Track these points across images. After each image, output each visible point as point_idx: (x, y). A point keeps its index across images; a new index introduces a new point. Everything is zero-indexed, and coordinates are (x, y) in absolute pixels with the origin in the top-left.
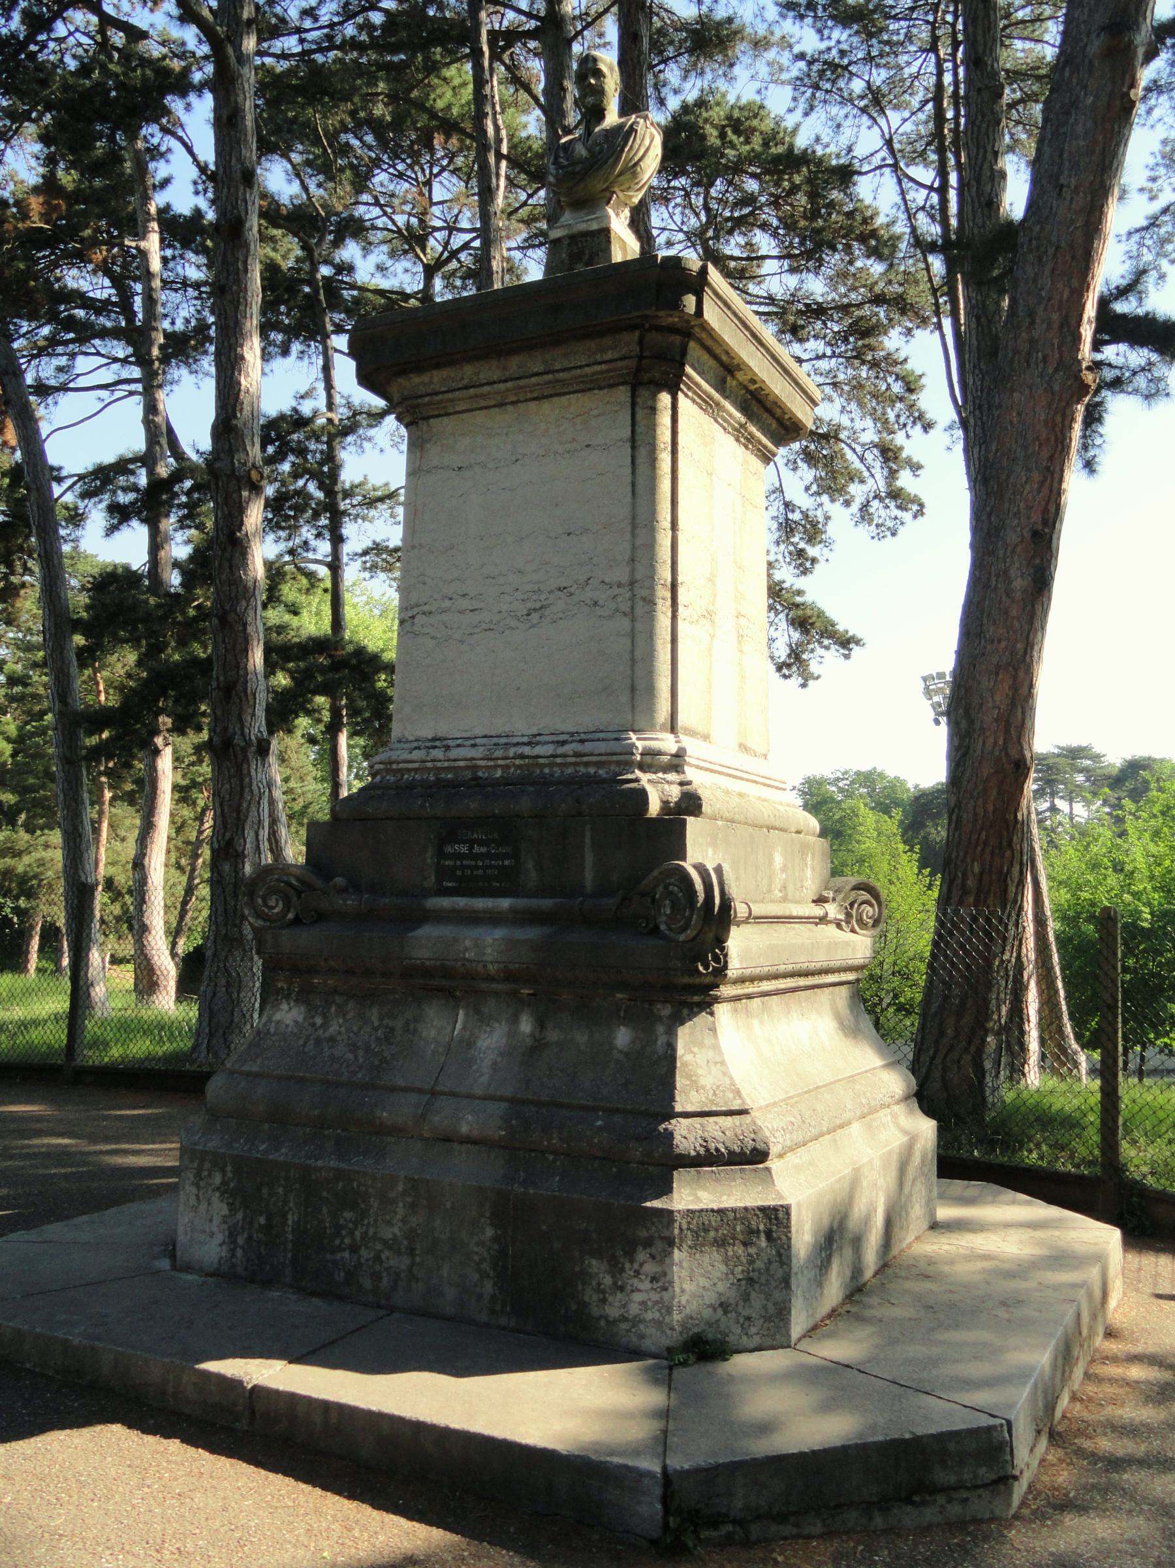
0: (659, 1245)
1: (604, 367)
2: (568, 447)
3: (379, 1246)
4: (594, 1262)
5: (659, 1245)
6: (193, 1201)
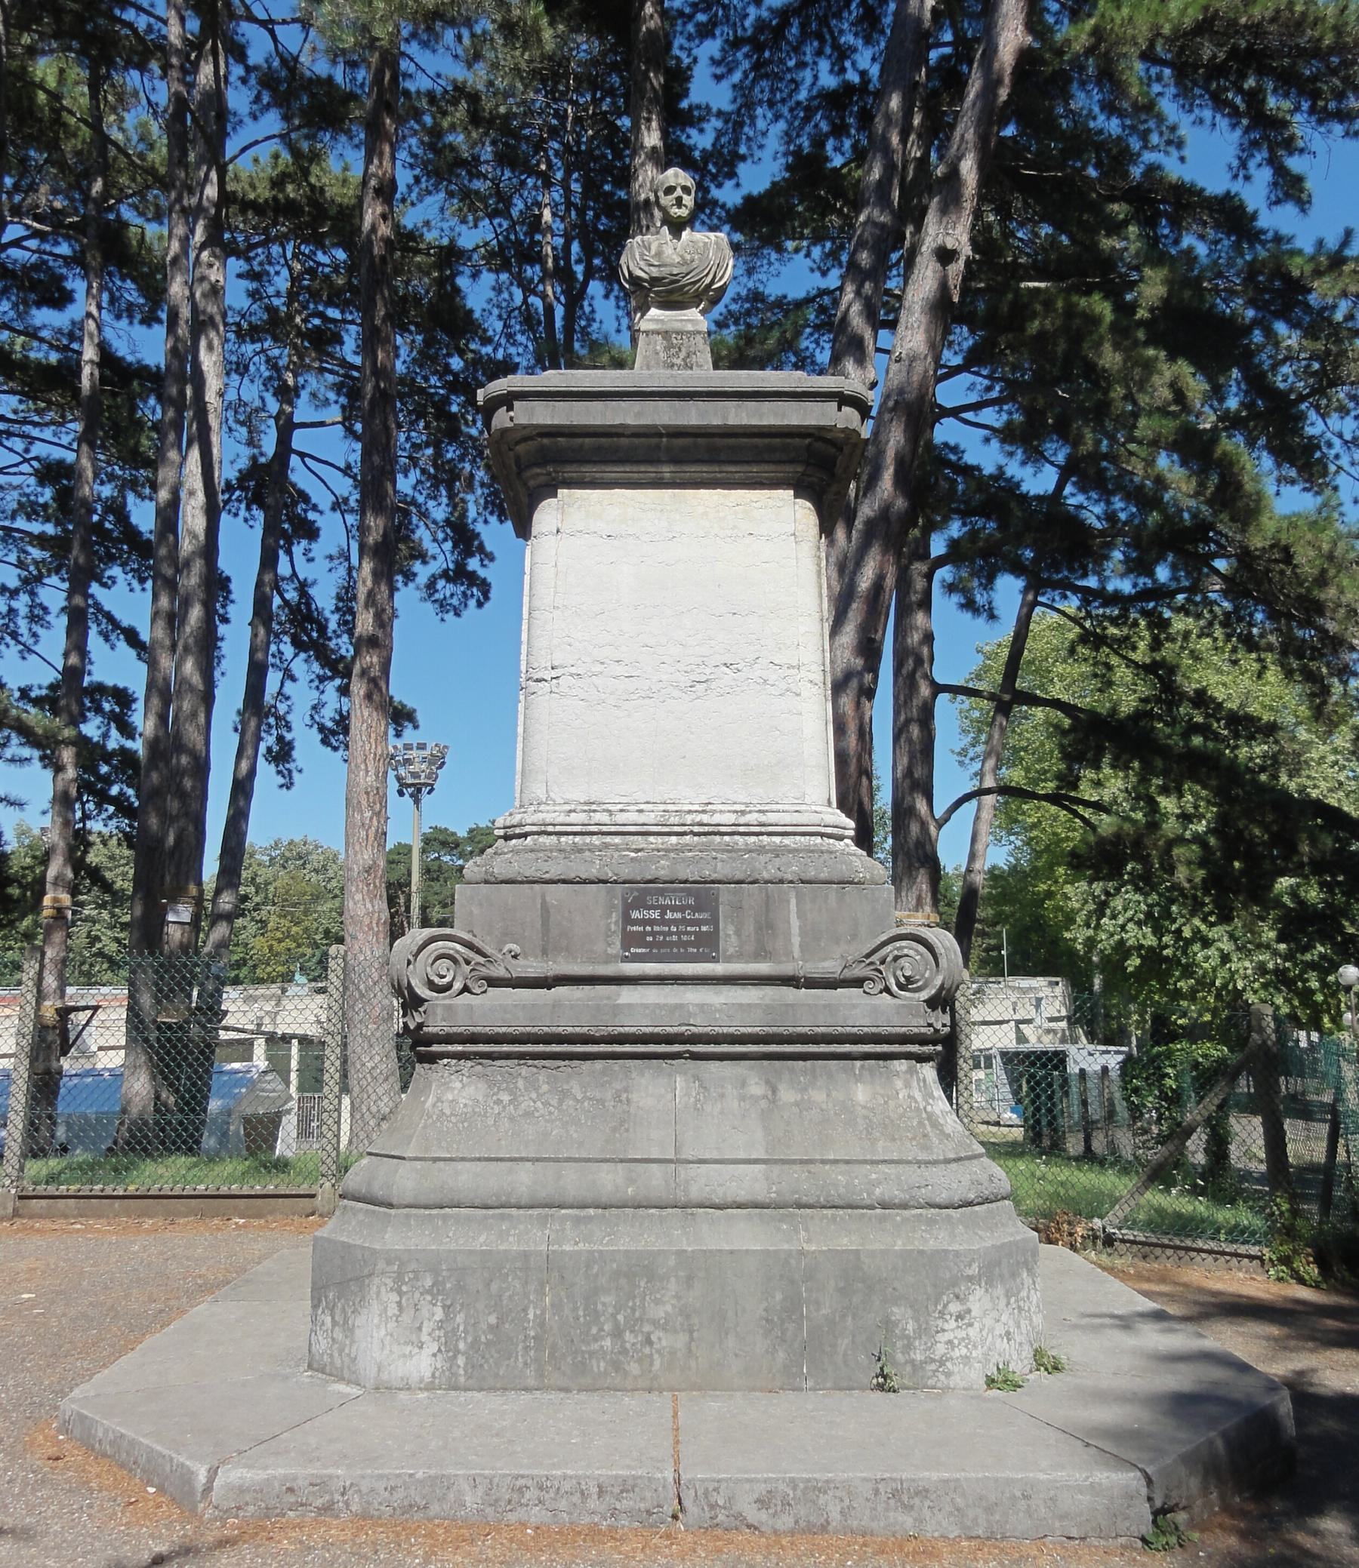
3: (647, 1328)
4: (895, 1309)
6: (393, 1310)
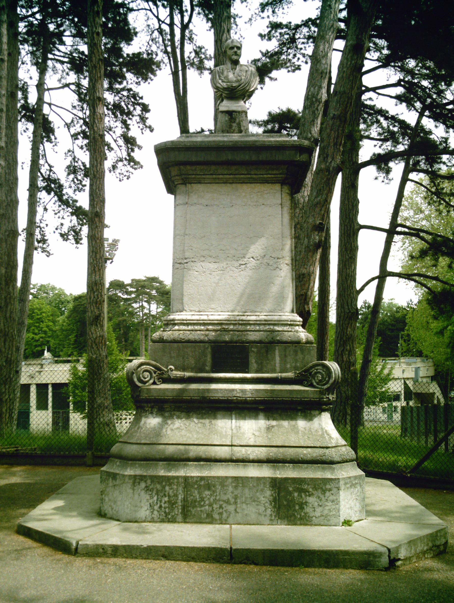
0: (335, 490)
1: (272, 176)
2: (255, 203)
3: (221, 503)
5: (335, 490)
